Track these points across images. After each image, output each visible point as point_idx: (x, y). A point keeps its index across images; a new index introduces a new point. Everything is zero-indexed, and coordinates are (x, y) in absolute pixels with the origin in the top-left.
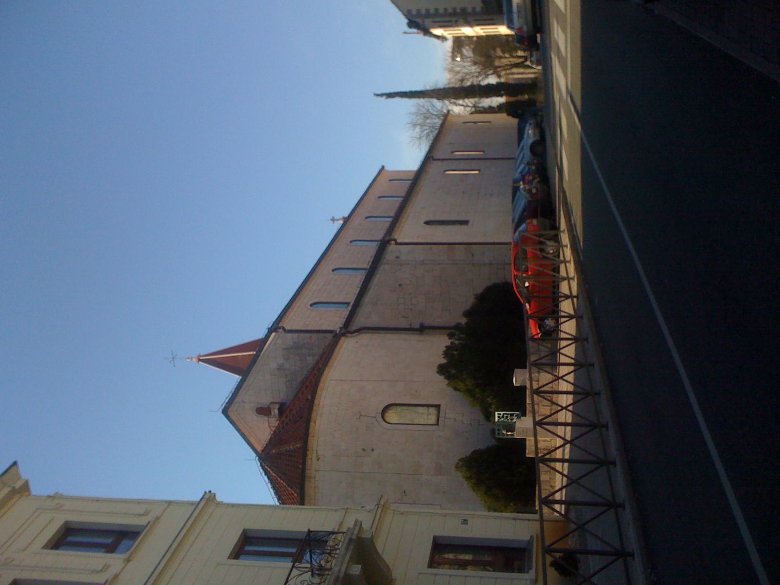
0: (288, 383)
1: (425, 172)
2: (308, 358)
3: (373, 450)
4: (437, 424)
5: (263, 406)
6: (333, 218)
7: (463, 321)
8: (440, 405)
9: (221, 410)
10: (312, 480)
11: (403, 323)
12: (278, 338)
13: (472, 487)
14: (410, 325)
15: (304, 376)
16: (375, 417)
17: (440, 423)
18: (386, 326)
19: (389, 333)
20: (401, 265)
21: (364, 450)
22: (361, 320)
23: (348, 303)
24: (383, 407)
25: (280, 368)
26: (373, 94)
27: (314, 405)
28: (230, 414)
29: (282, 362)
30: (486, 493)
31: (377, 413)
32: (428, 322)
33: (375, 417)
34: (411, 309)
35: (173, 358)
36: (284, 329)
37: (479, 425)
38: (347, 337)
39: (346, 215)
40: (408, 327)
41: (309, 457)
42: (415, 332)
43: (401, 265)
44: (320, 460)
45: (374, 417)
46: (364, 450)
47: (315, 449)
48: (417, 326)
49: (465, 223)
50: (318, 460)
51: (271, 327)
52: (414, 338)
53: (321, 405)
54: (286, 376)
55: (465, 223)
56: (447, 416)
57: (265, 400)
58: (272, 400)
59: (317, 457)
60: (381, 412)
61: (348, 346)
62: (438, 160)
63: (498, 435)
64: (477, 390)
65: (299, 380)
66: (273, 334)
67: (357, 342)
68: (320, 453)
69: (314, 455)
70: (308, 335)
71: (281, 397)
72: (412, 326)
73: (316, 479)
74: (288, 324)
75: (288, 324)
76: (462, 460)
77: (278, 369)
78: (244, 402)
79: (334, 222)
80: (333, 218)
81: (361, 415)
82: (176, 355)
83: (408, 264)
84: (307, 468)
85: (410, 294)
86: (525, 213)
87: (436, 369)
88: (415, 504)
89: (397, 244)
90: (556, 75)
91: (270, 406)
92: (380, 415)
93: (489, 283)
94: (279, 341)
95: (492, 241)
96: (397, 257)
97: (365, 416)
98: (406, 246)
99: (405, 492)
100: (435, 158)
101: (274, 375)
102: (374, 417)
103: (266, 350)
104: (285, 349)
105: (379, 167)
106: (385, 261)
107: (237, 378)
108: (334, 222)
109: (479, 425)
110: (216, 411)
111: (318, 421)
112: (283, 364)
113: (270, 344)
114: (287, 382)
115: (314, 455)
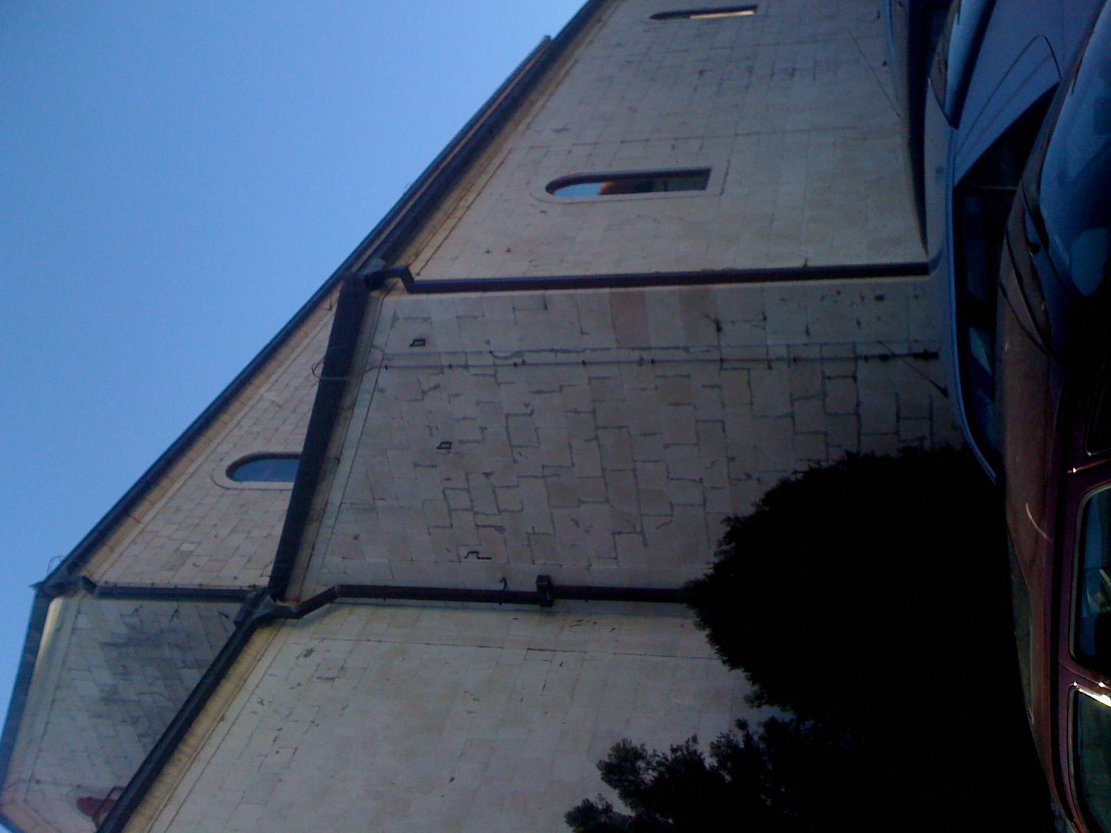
1: (599, 20)
2: (186, 673)
5: (94, 796)
11: (477, 576)
12: (79, 612)
14: (504, 580)
18: (421, 583)
19: (432, 607)
25: (110, 697)
32: (568, 573)
34: (500, 529)
43: (440, 369)
48: (531, 586)
49: (696, 178)
52: (522, 627)
54: (135, 721)
55: (696, 178)
61: (277, 659)
66: (55, 606)
67: (309, 653)
70: (168, 606)
72: (512, 587)
74: (105, 569)
75: (107, 568)
78: (38, 782)
85: (487, 475)
86: (1102, 685)
87: (597, 762)
89: (415, 287)
93: (783, 461)
94: (83, 622)
95: (797, 263)
96: (420, 342)
101: (99, 716)
106: (377, 355)
113: (58, 630)
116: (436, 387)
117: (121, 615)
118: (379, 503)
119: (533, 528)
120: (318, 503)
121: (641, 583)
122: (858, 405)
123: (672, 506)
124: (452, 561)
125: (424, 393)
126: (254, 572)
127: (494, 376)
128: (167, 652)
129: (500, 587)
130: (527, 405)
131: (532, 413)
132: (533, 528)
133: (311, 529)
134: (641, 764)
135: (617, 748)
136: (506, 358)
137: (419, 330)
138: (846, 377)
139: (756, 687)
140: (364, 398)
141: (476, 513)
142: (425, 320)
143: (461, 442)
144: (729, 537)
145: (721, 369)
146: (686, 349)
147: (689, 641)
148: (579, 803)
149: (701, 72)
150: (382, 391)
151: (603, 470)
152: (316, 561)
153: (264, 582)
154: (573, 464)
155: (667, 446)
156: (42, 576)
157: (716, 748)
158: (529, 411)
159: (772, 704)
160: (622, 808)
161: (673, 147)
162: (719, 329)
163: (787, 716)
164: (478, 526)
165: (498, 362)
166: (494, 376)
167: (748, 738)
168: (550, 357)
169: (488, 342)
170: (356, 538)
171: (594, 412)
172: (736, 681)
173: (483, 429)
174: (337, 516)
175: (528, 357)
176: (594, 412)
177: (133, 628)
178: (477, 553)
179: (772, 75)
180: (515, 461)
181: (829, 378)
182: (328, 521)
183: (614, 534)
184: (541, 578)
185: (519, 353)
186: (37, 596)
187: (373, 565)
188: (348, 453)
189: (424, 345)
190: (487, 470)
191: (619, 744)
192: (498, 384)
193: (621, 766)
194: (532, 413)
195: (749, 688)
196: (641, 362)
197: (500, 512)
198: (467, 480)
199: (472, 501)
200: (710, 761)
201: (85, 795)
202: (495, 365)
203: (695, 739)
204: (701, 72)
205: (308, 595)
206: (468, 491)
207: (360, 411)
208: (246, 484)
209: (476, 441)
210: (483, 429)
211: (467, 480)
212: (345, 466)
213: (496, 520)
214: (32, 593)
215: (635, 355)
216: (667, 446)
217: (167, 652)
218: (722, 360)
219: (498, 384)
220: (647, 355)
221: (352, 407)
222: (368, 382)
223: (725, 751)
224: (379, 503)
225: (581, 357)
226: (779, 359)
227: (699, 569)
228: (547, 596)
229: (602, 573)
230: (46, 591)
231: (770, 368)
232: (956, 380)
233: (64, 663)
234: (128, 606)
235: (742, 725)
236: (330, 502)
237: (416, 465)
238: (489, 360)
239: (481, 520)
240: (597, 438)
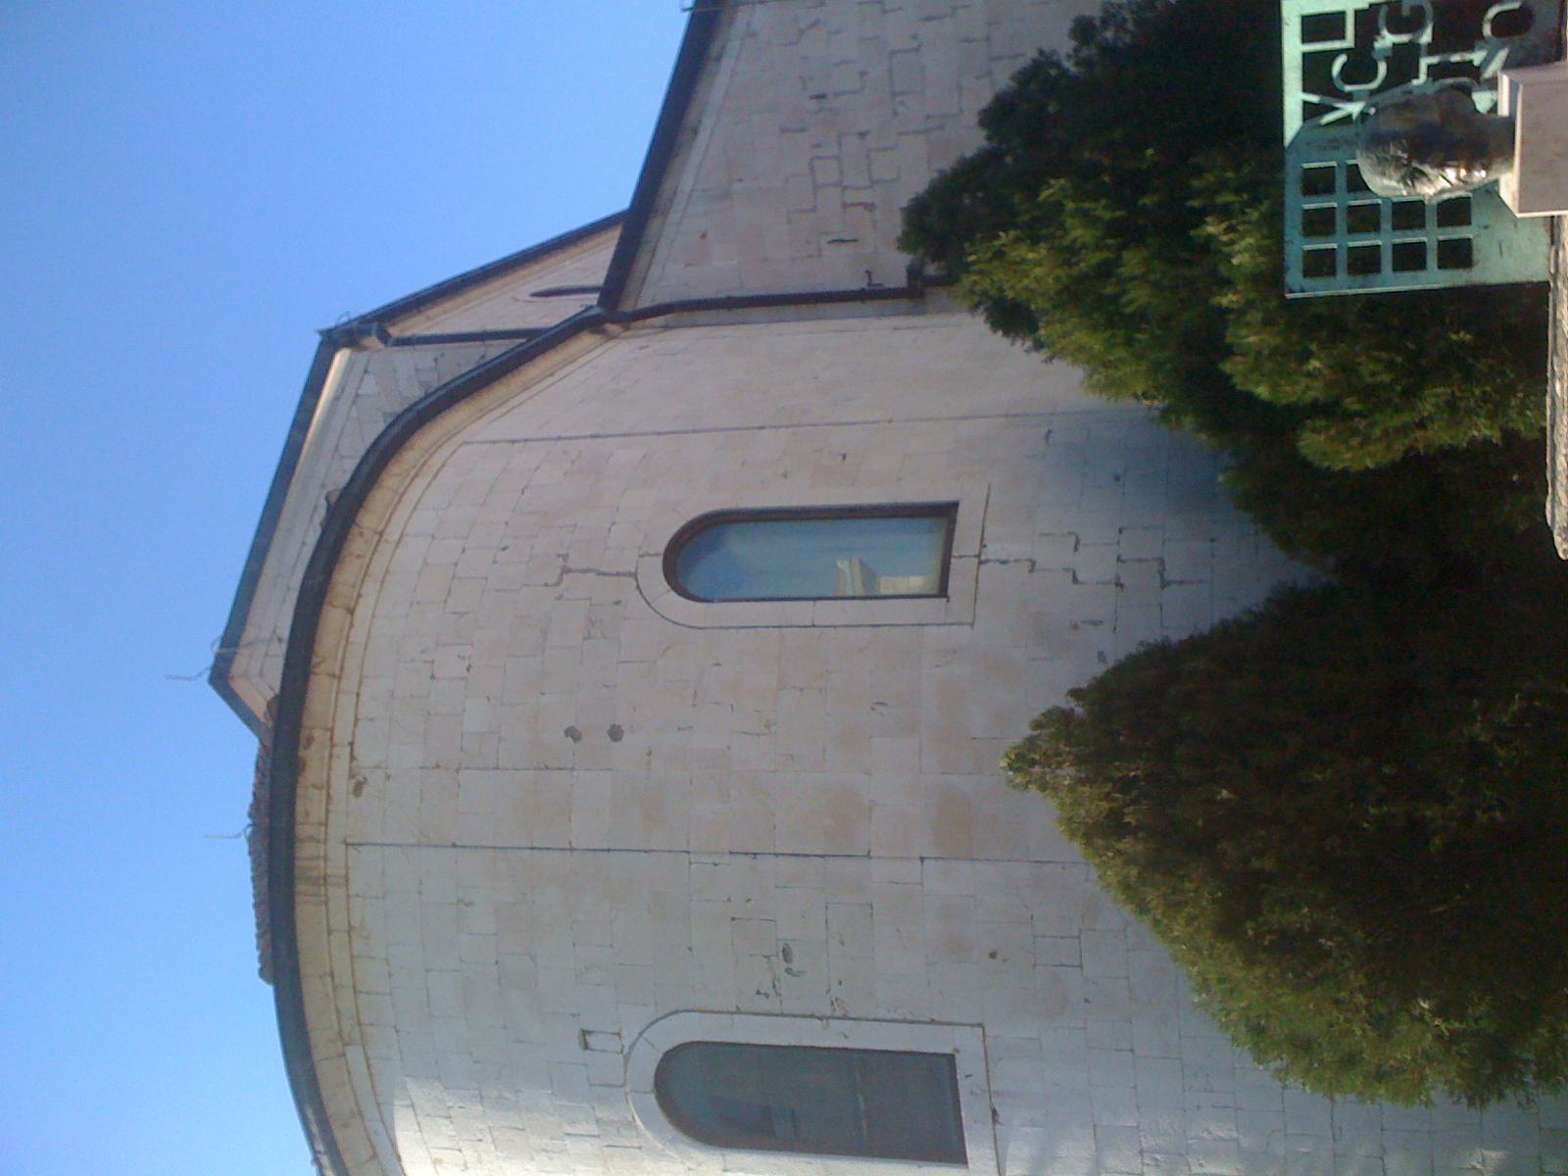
3: (615, 733)
4: (943, 592)
8: (953, 507)
10: (336, 893)
13: (1126, 886)
16: (634, 575)
17: (953, 585)
21: (573, 733)
22: (667, 274)
26: (1077, 553)
27: (355, 530)
28: (239, 686)
30: (1227, 928)
34: (869, 207)
37: (1164, 584)
38: (610, 337)
40: (858, 284)
41: (312, 774)
42: (890, 303)
44: (366, 790)
46: (573, 733)
47: (342, 735)
50: (358, 789)
53: (392, 534)
56: (992, 551)
59: (352, 776)
60: (661, 546)
63: (1308, 273)
64: (1133, 262)
66: (341, 358)
68: (367, 756)
69: (341, 766)
73: (354, 888)
81: (566, 571)
84: (302, 830)
85: (862, 135)
88: (845, 1018)
94: (370, 386)
99: (786, 954)
103: (326, 422)
109: (1164, 584)
111: (363, 611)
113: (336, 399)
115: (341, 766)
116: (815, 24)
117: (417, 370)
118: (737, 187)
119: (570, 843)
120: (667, 187)
124: (810, 256)
125: (802, 32)
130: (914, 37)
132: (570, 843)
133: (655, 223)
140: (733, 46)
141: (845, 188)
143: (837, 94)
150: (754, 35)
152: (655, 271)
154: (961, 111)
156: (330, 324)
158: (915, 44)
164: (845, 206)
170: (704, 236)
171: (988, 39)
174: (686, 208)
182: (674, 216)
186: (321, 344)
188: (708, 122)
191: (1305, 103)
197: (873, 183)
199: (841, 173)
205: (645, 302)
207: (727, 64)
210: (863, 73)
212: (703, 137)
213: (867, 196)
214: (318, 338)
221: (718, 59)
230: (334, 340)
233: (337, 448)
236: (679, 189)
237: (784, 130)
239: (852, 197)
240: (990, 73)
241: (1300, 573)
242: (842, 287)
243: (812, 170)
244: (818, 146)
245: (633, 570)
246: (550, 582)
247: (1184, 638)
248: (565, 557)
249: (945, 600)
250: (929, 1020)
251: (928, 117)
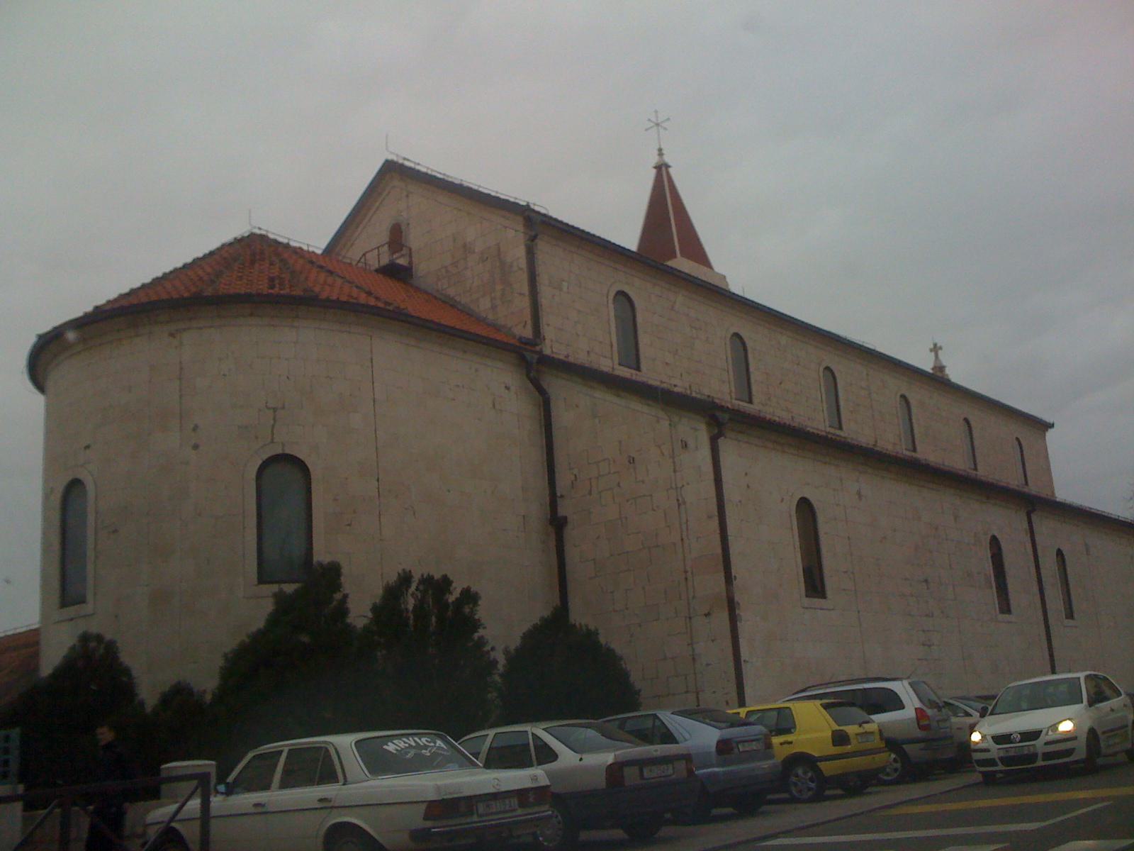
0: (443, 270)
3: (196, 447)
5: (404, 233)
6: (941, 348)
7: (476, 617)
9: (391, 157)
11: (563, 481)
15: (458, 299)
16: (272, 442)
20: (673, 457)
21: (195, 428)
23: (914, 450)
24: (302, 457)
25: (467, 249)
29: (476, 251)
31: (283, 445)
32: (571, 533)
33: (272, 442)
34: (590, 493)
35: (658, 125)
36: (533, 239)
39: (956, 374)
43: (673, 457)
45: (272, 439)
51: (533, 210)
57: (415, 239)
58: (413, 250)
60: (287, 451)
61: (498, 382)
62: (1030, 523)
65: (451, 292)
67: (507, 388)
71: (425, 269)
76: (111, 648)
77: (465, 246)
78: (407, 196)
79: (931, 350)
80: (941, 348)
82: (665, 129)
83: (675, 471)
85: (619, 485)
90: (879, 792)
91: (404, 248)
92: (278, 450)
96: (685, 445)
97: (275, 420)
98: (709, 460)
100: (1034, 517)
101: (454, 241)
102: (272, 439)
104: (499, 250)
105: (1047, 417)
107: (629, 238)
108: (931, 350)
110: (387, 149)
112: (474, 252)
114: (446, 267)
116: (663, 454)
118: (597, 420)
121: (569, 576)
122: (674, 695)
123: (612, 592)
126: (553, 346)
127: (672, 488)
128: (499, 287)
129: (559, 494)
131: (654, 510)
134: (471, 606)
135: (477, 593)
136: (681, 495)
137: (691, 444)
138: (687, 687)
139: (513, 651)
141: (597, 478)
142: (697, 447)
144: (588, 630)
145: (686, 617)
146: (694, 597)
147: (539, 611)
148: (451, 578)
149: (926, 581)
150: (658, 421)
151: (628, 552)
153: (547, 351)
155: (643, 588)
157: (481, 638)
158: (655, 508)
159: (506, 659)
160: (451, 599)
161: (846, 572)
162: (706, 615)
163: (500, 667)
164: (590, 479)
165: (679, 490)
166: (672, 488)
167: (488, 652)
168: (684, 520)
169: (688, 484)
170: (577, 406)
172: (515, 642)
173: (643, 482)
175: (682, 507)
176: (657, 546)
177: (511, 266)
178: (576, 480)
179: (924, 631)
180: (628, 501)
181: (686, 678)
183: (594, 560)
184: (565, 518)
185: (684, 503)
187: (563, 416)
189: (683, 448)
190: (621, 485)
192: (667, 491)
193: (469, 597)
194: (654, 510)
195: (512, 648)
196: (686, 572)
198: (615, 473)
200: (476, 636)
201: (403, 228)
202: (677, 488)
203: (485, 628)
204: (926, 581)
206: (609, 473)
207: (645, 409)
208: (611, 306)
209: (636, 478)
210: (643, 482)
211: (615, 473)
215: (689, 569)
216: (643, 588)
217: (499, 287)
218: (690, 618)
219: (667, 491)
220: (689, 574)
221: (648, 405)
222: (661, 414)
223: (482, 642)
224: (597, 420)
225: (685, 538)
226: (693, 650)
227: (579, 616)
228: (558, 524)
229: (572, 555)
231: (688, 645)
232: (636, 716)
234: (523, 263)
235: (493, 649)
237: (620, 442)
238: (680, 485)
241: (149, 709)
242: (558, 483)
243: (604, 460)
244: (614, 461)
245: (275, 441)
246: (268, 404)
247: (632, 679)
248: (283, 408)
249: (256, 583)
250: (562, 512)
251: (626, 518)
